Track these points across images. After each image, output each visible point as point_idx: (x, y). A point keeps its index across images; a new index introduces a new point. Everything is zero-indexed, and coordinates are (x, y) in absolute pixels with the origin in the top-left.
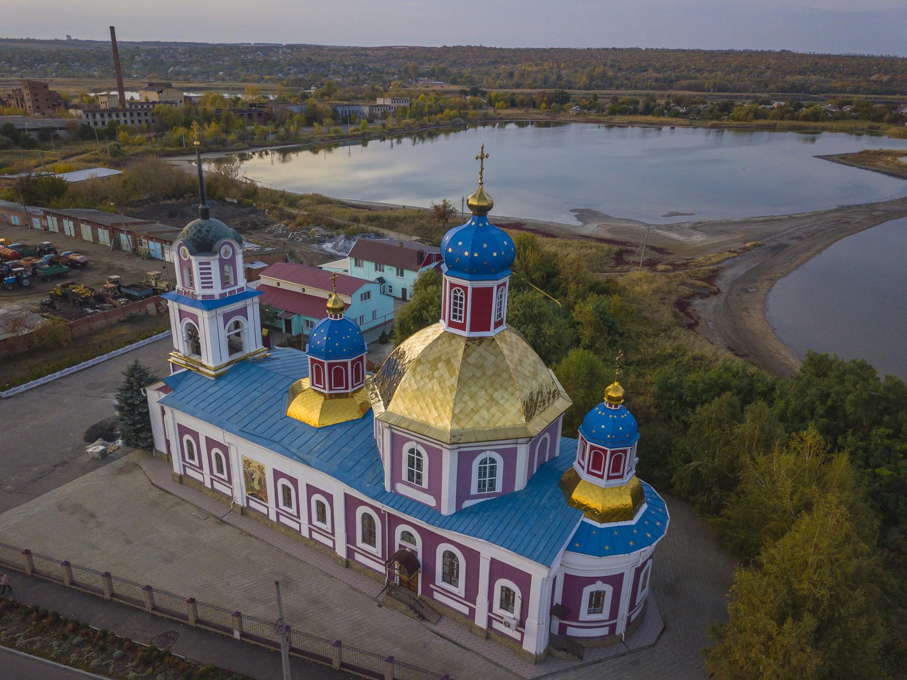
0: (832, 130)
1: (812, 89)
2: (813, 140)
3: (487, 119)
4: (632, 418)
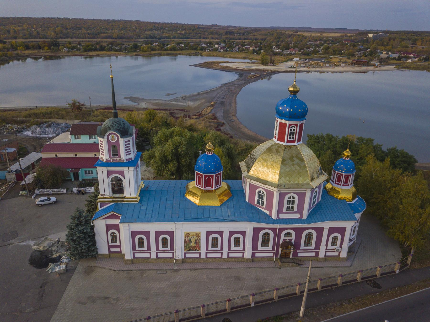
0: (182, 54)
1: (158, 37)
2: (176, 59)
3: (19, 56)
4: (353, 163)
